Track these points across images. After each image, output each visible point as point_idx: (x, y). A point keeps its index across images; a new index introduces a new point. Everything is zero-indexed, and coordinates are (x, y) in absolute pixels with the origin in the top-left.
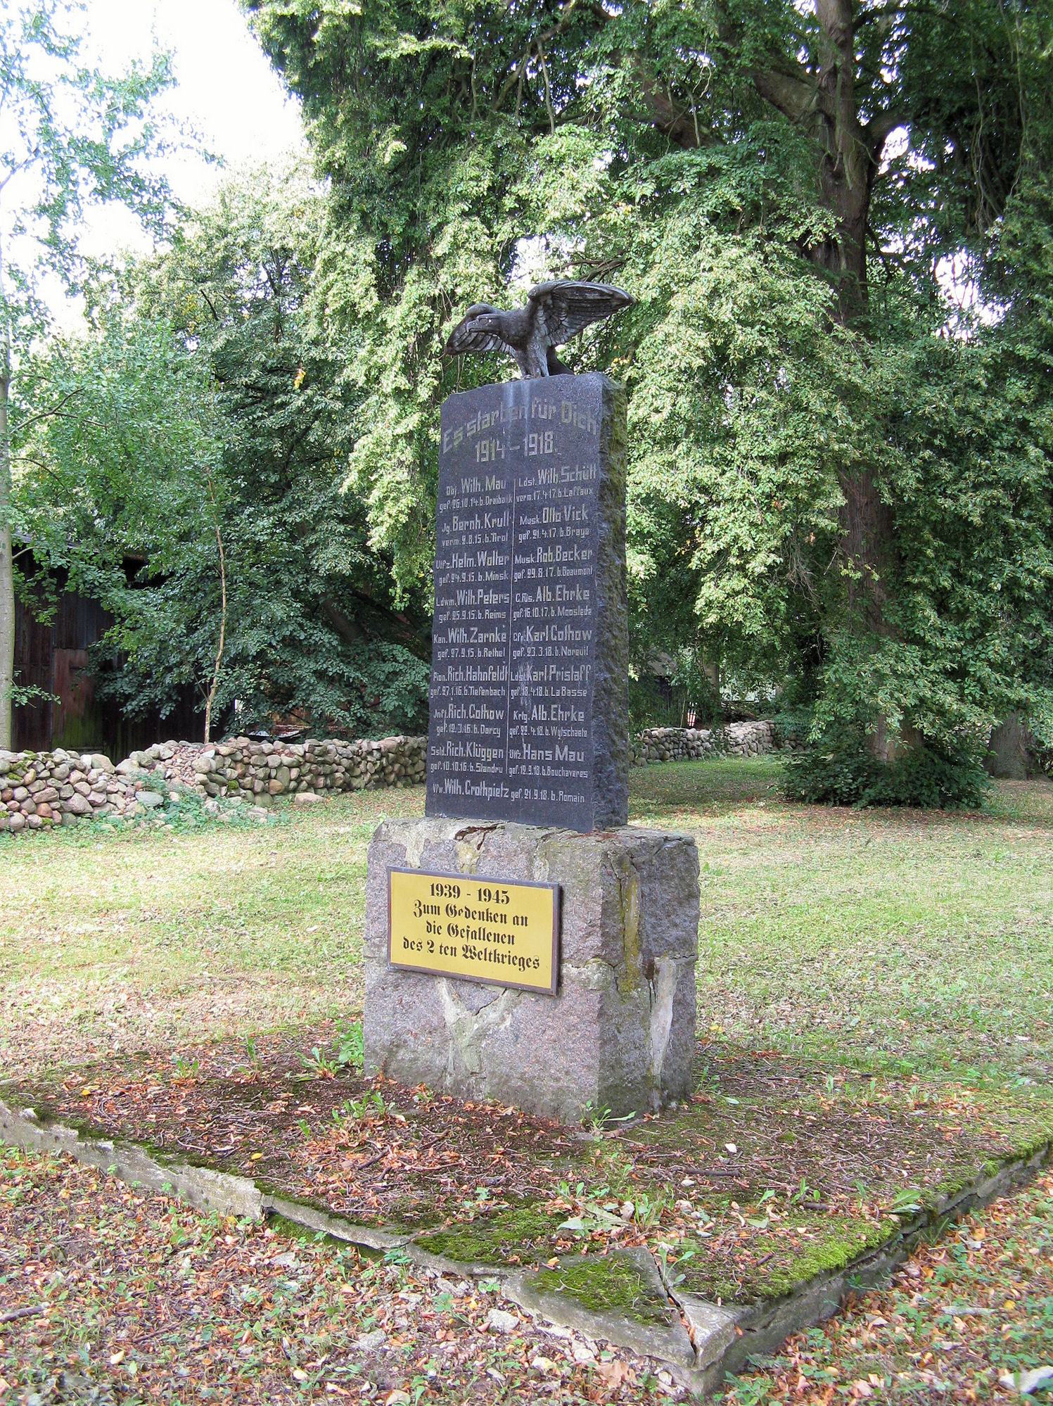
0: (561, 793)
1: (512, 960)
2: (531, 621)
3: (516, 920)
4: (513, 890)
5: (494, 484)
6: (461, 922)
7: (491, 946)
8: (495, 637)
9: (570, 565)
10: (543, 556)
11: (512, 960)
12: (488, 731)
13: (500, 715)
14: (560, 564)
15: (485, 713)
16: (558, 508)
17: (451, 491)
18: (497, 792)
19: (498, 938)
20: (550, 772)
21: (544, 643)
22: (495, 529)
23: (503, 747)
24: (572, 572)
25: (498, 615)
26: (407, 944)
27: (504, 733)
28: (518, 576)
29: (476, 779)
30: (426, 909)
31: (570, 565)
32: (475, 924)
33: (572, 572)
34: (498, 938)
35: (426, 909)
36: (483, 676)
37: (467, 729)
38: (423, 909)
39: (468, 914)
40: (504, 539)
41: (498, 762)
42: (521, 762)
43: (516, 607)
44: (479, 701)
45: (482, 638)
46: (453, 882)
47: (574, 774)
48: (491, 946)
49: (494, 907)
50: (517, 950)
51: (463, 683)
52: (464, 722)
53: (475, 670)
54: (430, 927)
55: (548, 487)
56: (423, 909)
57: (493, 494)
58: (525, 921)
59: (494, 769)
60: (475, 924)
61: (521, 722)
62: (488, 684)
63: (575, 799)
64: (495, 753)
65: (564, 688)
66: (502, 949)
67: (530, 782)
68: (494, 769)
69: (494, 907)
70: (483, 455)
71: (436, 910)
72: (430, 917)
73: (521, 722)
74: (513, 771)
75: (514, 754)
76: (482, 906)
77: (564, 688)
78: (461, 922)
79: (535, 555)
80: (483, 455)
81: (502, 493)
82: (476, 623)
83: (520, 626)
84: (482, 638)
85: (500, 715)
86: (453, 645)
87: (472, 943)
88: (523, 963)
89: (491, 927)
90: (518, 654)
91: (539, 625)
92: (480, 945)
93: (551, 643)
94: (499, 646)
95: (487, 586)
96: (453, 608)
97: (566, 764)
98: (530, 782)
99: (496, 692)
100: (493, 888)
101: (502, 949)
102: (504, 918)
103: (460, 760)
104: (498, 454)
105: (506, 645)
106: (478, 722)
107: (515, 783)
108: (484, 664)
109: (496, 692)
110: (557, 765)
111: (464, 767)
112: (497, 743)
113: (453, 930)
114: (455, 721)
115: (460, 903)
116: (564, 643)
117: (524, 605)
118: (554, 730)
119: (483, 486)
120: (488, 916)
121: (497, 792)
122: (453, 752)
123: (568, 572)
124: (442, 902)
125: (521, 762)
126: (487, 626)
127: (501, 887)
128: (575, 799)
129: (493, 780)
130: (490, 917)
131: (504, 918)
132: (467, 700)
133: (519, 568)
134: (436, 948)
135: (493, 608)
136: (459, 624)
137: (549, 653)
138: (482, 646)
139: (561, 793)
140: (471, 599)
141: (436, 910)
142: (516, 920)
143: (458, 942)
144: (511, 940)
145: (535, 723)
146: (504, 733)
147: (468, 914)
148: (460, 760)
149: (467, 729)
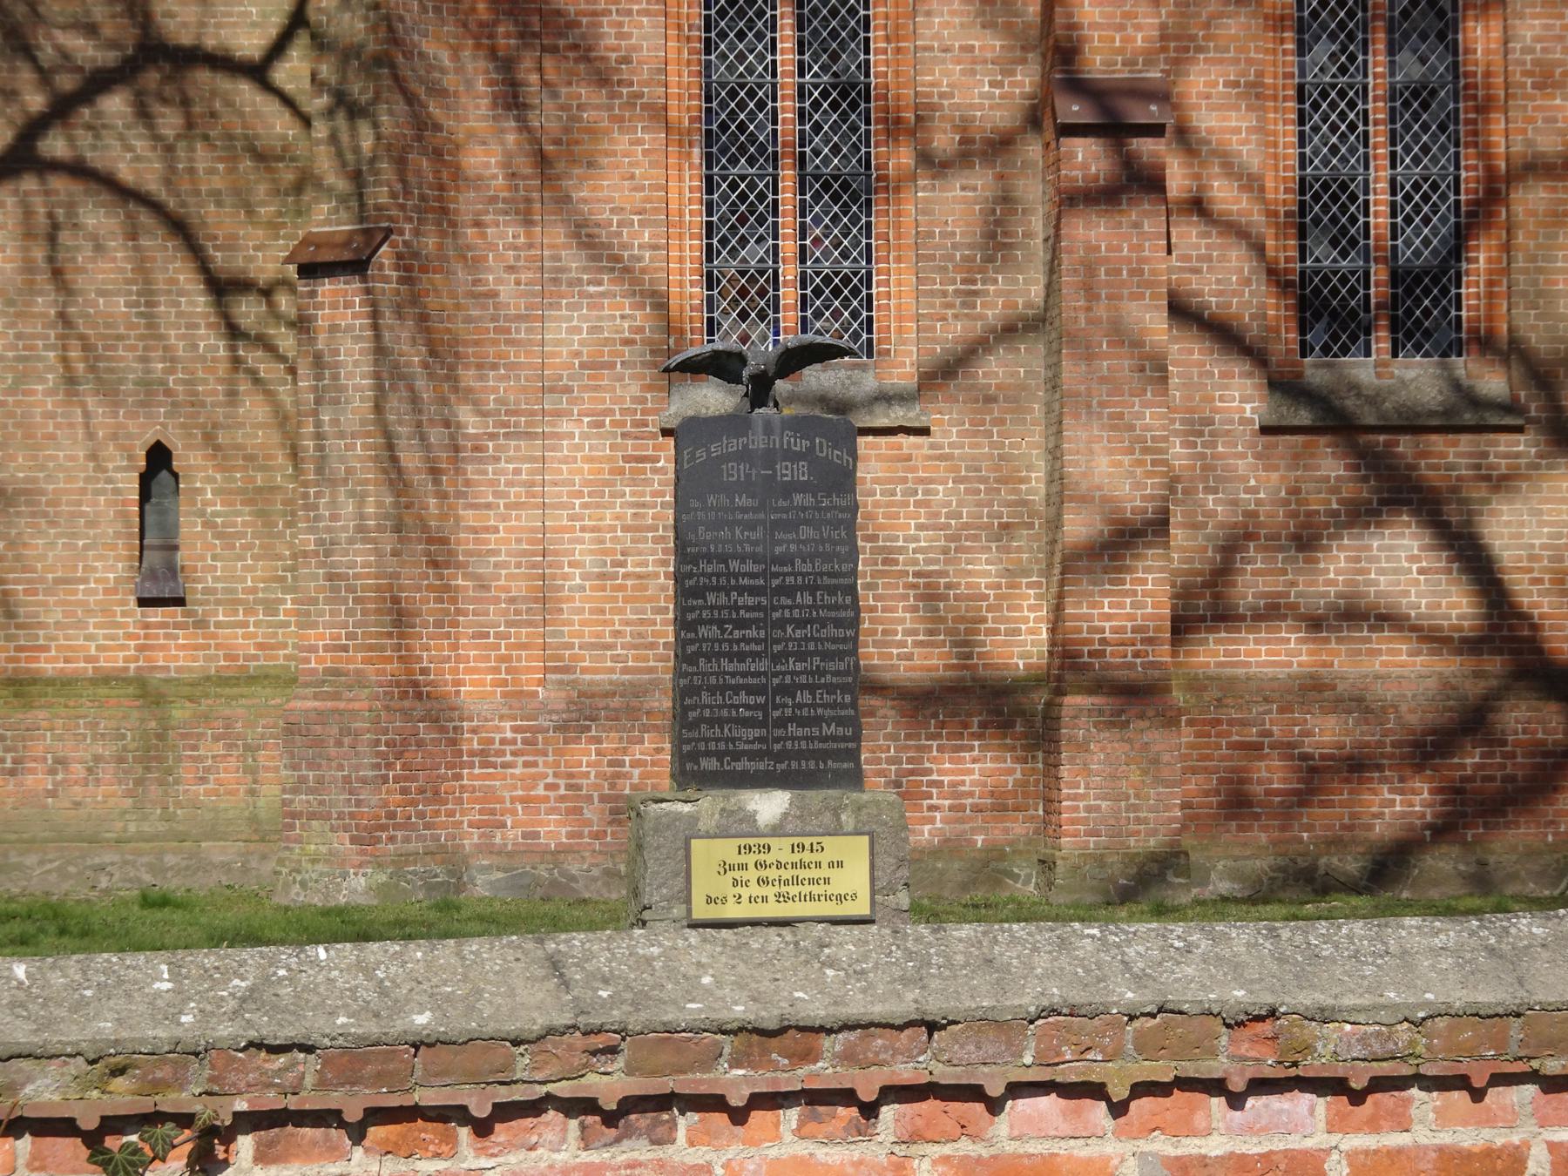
0: (830, 762)
1: (829, 898)
2: (791, 621)
3: (831, 865)
4: (826, 841)
5: (742, 501)
6: (772, 873)
7: (806, 889)
8: (752, 633)
9: (831, 575)
10: (711, 598)
11: (829, 898)
12: (748, 714)
13: (761, 700)
14: (821, 574)
15: (743, 697)
16: (817, 528)
17: (694, 504)
18: (762, 766)
19: (811, 881)
20: (818, 745)
21: (806, 639)
22: (748, 540)
23: (766, 727)
24: (834, 581)
25: (756, 615)
26: (709, 900)
27: (766, 715)
28: (775, 582)
29: (736, 756)
30: (732, 868)
31: (831, 575)
32: (786, 874)
33: (834, 581)
34: (811, 881)
35: (732, 868)
36: (742, 667)
37: (725, 713)
38: (726, 867)
39: (779, 865)
40: (760, 549)
41: (761, 740)
42: (786, 739)
43: (774, 609)
44: (736, 689)
45: (737, 634)
46: (762, 841)
47: (842, 746)
48: (806, 889)
49: (807, 857)
50: (831, 890)
51: (717, 674)
52: (720, 707)
53: (731, 661)
54: (735, 883)
55: (804, 509)
56: (726, 867)
57: (744, 510)
58: (840, 864)
59: (756, 746)
60: (786, 874)
61: (785, 706)
62: (744, 675)
63: (845, 766)
64: (757, 733)
65: (828, 677)
66: (816, 890)
67: (799, 755)
68: (756, 746)
69: (807, 857)
70: (783, 475)
71: (744, 867)
72: (737, 874)
73: (785, 706)
74: (777, 747)
75: (779, 732)
76: (796, 858)
77: (828, 677)
78: (772, 873)
79: (793, 565)
80: (783, 475)
81: (755, 510)
82: (730, 621)
83: (781, 624)
84: (737, 634)
85: (761, 700)
86: (704, 640)
87: (784, 889)
88: (840, 898)
89: (804, 874)
90: (777, 648)
91: (801, 623)
92: (793, 890)
93: (813, 639)
94: (757, 641)
95: (741, 590)
96: (701, 608)
97: (834, 739)
98: (799, 755)
99: (755, 681)
100: (807, 841)
101: (816, 890)
102: (818, 865)
103: (717, 740)
104: (748, 476)
105: (765, 640)
106: (737, 707)
107: (779, 757)
108: (741, 656)
109: (755, 681)
110: (825, 739)
111: (722, 746)
112: (763, 724)
113: (762, 882)
114: (710, 707)
115: (769, 858)
116: (827, 640)
117: (783, 607)
118: (820, 711)
119: (733, 502)
120: (802, 865)
121: (762, 766)
122: (709, 734)
123: (827, 581)
124: (751, 859)
125: (786, 739)
126: (741, 624)
127: (815, 840)
128: (845, 766)
129: (752, 755)
130: (802, 865)
131: (818, 865)
132: (723, 689)
133: (776, 575)
134: (745, 899)
135: (748, 609)
136: (711, 622)
137: (811, 646)
138: (738, 641)
139: (830, 762)
140: (723, 599)
141: (744, 867)
142: (831, 865)
143: (770, 891)
144: (827, 881)
145: (800, 706)
146: (766, 715)
147: (779, 865)
148: (717, 740)
149: (725, 713)
